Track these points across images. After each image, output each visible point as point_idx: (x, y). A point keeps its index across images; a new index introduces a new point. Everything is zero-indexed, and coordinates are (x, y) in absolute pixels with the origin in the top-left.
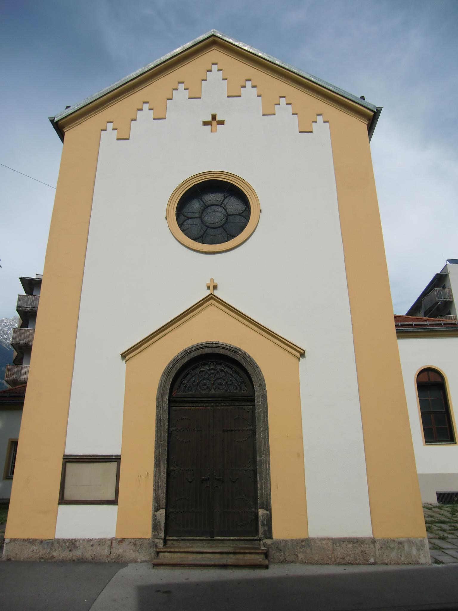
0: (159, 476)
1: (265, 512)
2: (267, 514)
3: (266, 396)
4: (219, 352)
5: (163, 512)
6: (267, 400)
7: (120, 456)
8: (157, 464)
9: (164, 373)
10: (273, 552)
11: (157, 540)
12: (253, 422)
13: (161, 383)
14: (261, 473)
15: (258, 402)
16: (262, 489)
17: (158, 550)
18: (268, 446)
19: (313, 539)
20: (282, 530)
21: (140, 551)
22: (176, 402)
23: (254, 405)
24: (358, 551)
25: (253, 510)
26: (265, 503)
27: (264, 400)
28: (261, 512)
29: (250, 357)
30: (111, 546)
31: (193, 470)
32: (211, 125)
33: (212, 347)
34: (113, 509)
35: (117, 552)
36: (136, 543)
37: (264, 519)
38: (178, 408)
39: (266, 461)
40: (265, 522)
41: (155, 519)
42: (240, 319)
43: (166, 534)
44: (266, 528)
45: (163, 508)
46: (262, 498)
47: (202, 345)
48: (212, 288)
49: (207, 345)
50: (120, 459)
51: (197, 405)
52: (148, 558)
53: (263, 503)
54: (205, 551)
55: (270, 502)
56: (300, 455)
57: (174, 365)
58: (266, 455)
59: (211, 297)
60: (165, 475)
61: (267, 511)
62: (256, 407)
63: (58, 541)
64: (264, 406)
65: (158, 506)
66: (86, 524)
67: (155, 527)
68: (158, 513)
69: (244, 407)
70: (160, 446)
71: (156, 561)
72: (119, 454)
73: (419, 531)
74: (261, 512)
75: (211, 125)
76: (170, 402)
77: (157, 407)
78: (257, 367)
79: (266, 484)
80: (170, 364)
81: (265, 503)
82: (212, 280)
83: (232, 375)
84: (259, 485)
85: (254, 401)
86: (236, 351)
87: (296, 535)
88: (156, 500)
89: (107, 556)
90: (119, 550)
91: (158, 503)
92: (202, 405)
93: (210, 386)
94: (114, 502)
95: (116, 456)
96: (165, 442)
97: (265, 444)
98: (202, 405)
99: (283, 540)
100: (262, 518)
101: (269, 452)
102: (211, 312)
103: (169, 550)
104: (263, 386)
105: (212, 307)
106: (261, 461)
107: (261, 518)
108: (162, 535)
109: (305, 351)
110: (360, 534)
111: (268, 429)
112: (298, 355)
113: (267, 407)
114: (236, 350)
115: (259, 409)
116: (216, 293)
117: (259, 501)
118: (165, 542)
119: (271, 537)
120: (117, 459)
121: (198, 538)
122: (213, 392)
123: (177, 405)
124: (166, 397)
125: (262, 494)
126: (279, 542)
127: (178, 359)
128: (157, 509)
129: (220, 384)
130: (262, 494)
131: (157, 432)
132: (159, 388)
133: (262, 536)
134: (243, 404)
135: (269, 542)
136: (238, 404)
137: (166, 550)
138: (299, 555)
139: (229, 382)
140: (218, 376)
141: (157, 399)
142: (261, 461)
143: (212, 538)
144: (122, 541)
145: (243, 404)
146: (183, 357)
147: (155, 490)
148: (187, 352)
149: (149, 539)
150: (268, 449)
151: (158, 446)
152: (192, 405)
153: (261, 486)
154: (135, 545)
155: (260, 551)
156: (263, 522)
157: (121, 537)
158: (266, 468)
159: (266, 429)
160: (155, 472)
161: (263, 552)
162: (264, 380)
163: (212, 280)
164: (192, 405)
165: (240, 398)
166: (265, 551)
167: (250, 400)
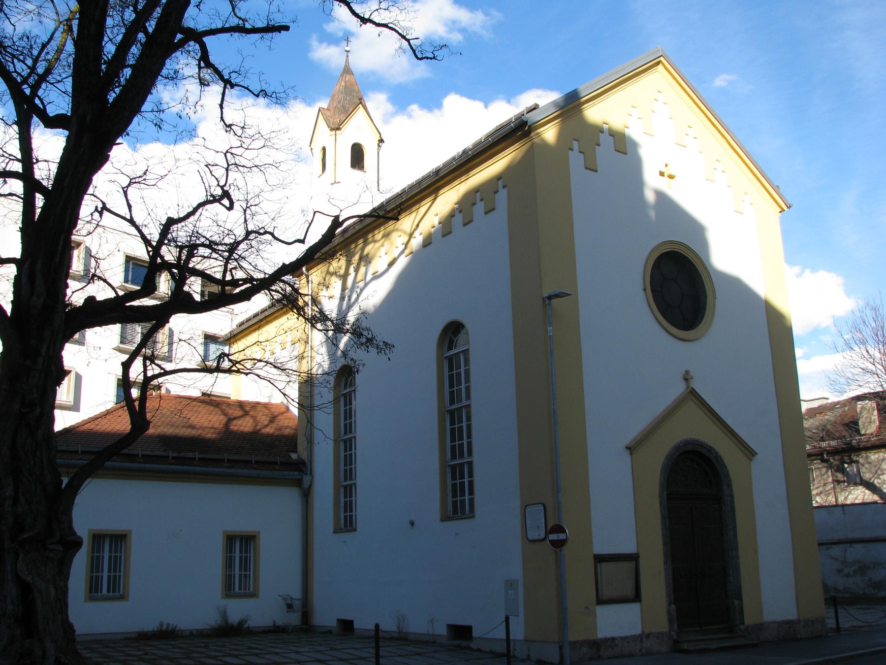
8: (666, 562)
20: (749, 619)
34: (635, 608)
63: (601, 640)
66: (618, 622)
67: (670, 621)
74: (736, 602)
135: (742, 627)
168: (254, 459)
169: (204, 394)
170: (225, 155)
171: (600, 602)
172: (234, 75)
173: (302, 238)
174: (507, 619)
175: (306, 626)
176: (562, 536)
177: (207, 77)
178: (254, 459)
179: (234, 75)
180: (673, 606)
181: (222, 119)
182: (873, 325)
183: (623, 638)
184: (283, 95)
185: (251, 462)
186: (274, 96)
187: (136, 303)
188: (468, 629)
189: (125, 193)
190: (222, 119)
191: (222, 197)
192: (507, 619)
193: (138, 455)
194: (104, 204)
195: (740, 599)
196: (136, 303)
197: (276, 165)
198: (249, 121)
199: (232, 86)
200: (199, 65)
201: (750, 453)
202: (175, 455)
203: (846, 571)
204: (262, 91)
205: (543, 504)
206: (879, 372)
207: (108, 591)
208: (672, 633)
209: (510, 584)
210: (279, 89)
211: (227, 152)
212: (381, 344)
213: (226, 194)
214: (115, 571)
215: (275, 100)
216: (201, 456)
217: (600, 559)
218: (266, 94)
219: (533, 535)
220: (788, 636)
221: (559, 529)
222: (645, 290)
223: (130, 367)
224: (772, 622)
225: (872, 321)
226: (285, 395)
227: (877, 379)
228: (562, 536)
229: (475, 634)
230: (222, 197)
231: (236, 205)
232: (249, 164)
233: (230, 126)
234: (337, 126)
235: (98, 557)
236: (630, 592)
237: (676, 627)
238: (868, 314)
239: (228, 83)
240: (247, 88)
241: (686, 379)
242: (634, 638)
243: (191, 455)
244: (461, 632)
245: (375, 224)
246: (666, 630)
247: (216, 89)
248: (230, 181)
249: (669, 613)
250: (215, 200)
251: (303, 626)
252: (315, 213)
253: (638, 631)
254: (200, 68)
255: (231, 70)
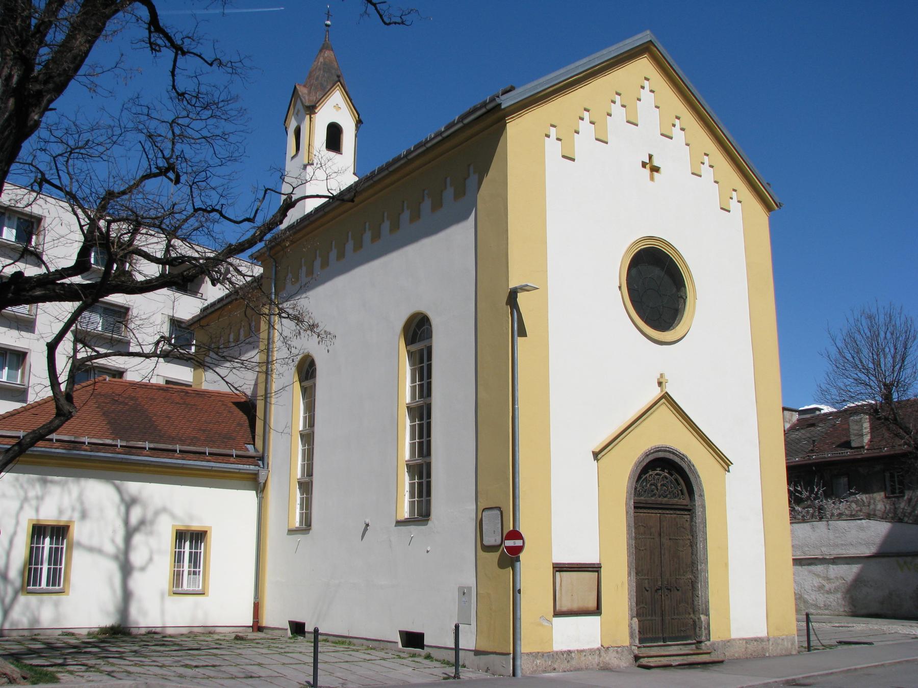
8: (629, 574)
12: (693, 533)
19: (734, 640)
20: (716, 635)
24: (760, 647)
32: (259, 487)
34: (596, 619)
36: (618, 649)
42: (606, 451)
63: (557, 653)
66: (577, 635)
67: (632, 635)
73: (795, 632)
74: (703, 617)
75: (259, 487)
87: (724, 637)
110: (760, 635)
135: (708, 643)
167: (689, 510)
168: (207, 450)
169: (168, 382)
170: (171, 125)
171: (557, 614)
172: (187, 41)
173: (252, 217)
174: (457, 627)
175: (257, 627)
176: (518, 543)
177: (160, 42)
178: (207, 450)
179: (187, 41)
180: (635, 620)
181: (174, 87)
182: (868, 334)
183: (580, 652)
184: (239, 65)
185: (205, 453)
186: (229, 65)
187: (67, 281)
188: (421, 636)
189: (265, 193)
190: (174, 87)
191: (167, 170)
192: (457, 627)
193: (84, 443)
194: (43, 174)
195: (707, 615)
196: (67, 281)
197: (224, 136)
198: (203, 89)
199: (184, 53)
200: (149, 29)
201: (726, 463)
202: (124, 444)
203: (827, 587)
204: (215, 60)
205: (499, 508)
206: (872, 384)
207: (48, 585)
208: (633, 647)
209: (464, 592)
210: (235, 58)
211: (173, 121)
212: (322, 332)
213: (171, 168)
214: (56, 564)
215: (230, 70)
216: (152, 446)
217: (560, 568)
218: (221, 63)
219: (490, 540)
220: (755, 654)
221: (515, 534)
222: (620, 287)
223: (56, 348)
224: (740, 639)
225: (867, 331)
226: (227, 383)
227: (870, 391)
228: (518, 543)
229: (427, 641)
230: (167, 170)
231: (183, 179)
232: (197, 135)
233: (183, 94)
234: (312, 104)
235: (38, 548)
236: (592, 604)
237: (637, 641)
238: (864, 324)
239: (179, 50)
240: (200, 56)
241: (660, 384)
242: (592, 652)
243: (140, 444)
244: (413, 640)
245: (331, 207)
246: (627, 643)
247: (168, 54)
248: (177, 153)
249: (630, 626)
250: (163, 172)
251: (118, 635)
252: (266, 191)
253: (597, 645)
254: (150, 32)
255: (185, 34)
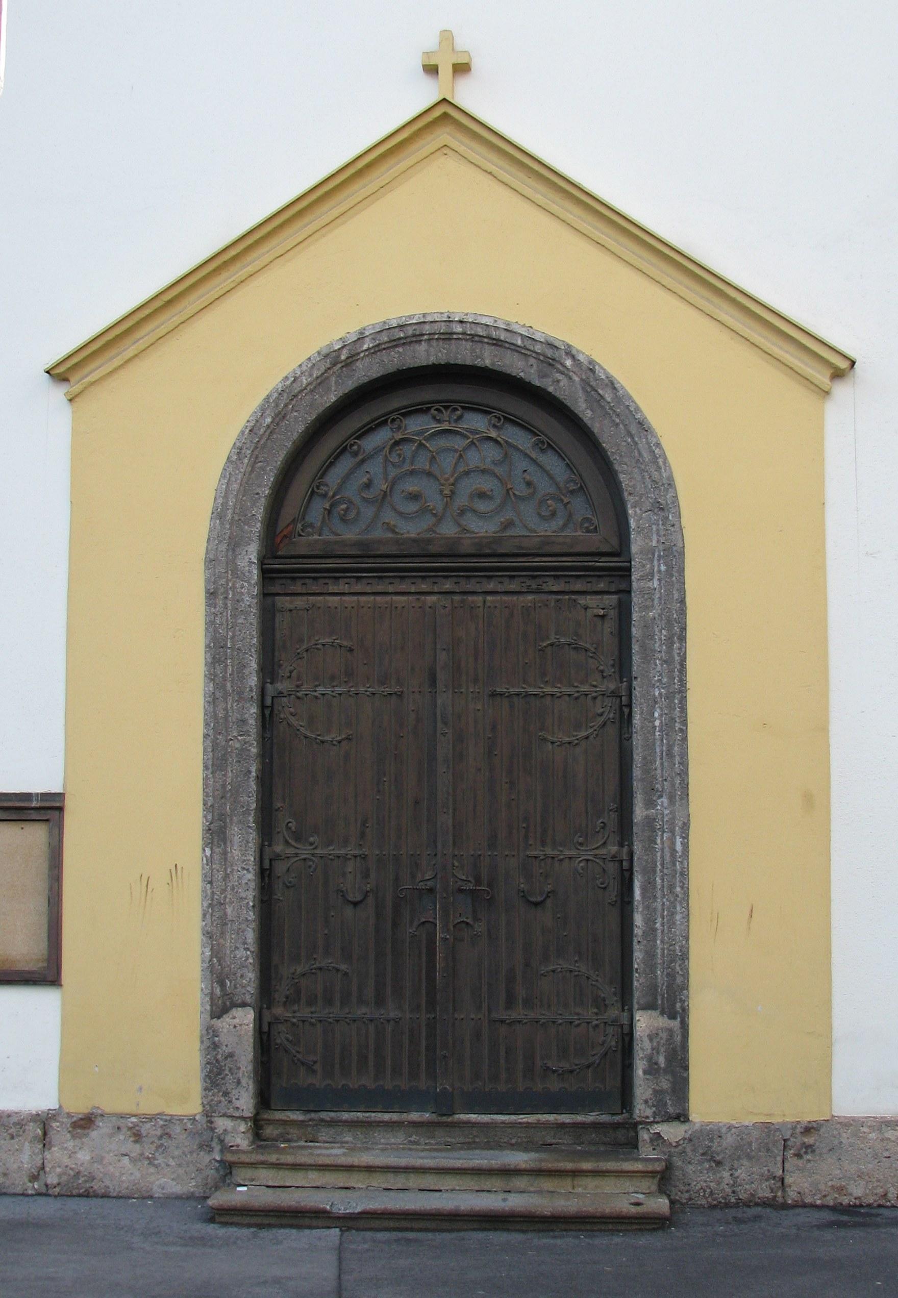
0: (226, 877)
1: (663, 1022)
2: (670, 1031)
3: (682, 554)
4: (478, 362)
5: (245, 1018)
6: (682, 571)
7: (60, 796)
8: (216, 834)
9: (239, 450)
10: (690, 1169)
11: (222, 1124)
13: (224, 495)
14: (650, 871)
15: (645, 580)
16: (651, 931)
17: (229, 1157)
18: (684, 763)
20: (728, 1079)
21: (160, 1160)
22: (293, 575)
23: (629, 592)
25: (614, 1012)
26: (662, 988)
27: (670, 567)
28: (645, 1023)
29: (612, 384)
30: (45, 1140)
31: (364, 857)
33: (448, 337)
34: (37, 1006)
35: (66, 1161)
37: (656, 1050)
38: (299, 602)
39: (672, 822)
40: (662, 1060)
41: (215, 1046)
43: (264, 1100)
44: (665, 1084)
45: (244, 1005)
46: (651, 967)
47: (401, 327)
48: (446, 71)
49: (427, 329)
50: (61, 809)
51: (380, 588)
52: (191, 1186)
53: (653, 988)
54: (418, 1162)
55: (685, 987)
56: (814, 802)
57: (280, 417)
58: (672, 799)
59: (444, 116)
60: (250, 876)
61: (672, 1017)
62: (636, 599)
64: (669, 593)
65: (225, 994)
67: (216, 1073)
68: (224, 1024)
69: (582, 600)
70: (224, 758)
71: (219, 1199)
72: (57, 789)
76: (267, 574)
77: (211, 595)
78: (643, 426)
79: (672, 914)
80: (263, 409)
81: (662, 988)
82: (447, 37)
83: (534, 461)
84: (638, 919)
85: (626, 573)
86: (551, 355)
88: (218, 973)
89: (34, 1178)
90: (69, 1156)
91: (222, 984)
92: (403, 587)
93: (435, 502)
94: (47, 975)
95: (46, 796)
96: (249, 741)
97: (670, 755)
98: (403, 587)
99: (730, 1127)
100: (647, 1045)
101: (685, 786)
102: (447, 182)
103: (273, 1158)
104: (665, 508)
105: (450, 164)
106: (650, 822)
107: (642, 1048)
108: (245, 1101)
109: (853, 363)
111: (683, 690)
112: (822, 377)
113: (683, 601)
114: (549, 352)
115: (647, 608)
116: (470, 97)
117: (638, 982)
118: (257, 1125)
119: (682, 1117)
120: (43, 810)
121: (386, 1117)
122: (448, 530)
123: (298, 587)
124: (251, 553)
125: (650, 955)
126: (712, 1133)
127: (297, 388)
128: (220, 1007)
129: (482, 495)
130: (650, 955)
131: (212, 700)
132: (219, 515)
133: (649, 1112)
134: (578, 586)
135: (672, 1132)
136: (448, 586)
137: (261, 1158)
138: (789, 1180)
139: (521, 490)
140: (473, 459)
141: (211, 562)
142: (650, 822)
143: (444, 1119)
144: (85, 1123)
145: (578, 586)
146: (321, 382)
147: (208, 935)
148: (338, 360)
149: (193, 1120)
150: (684, 774)
151: (217, 760)
152: (358, 588)
153: (650, 922)
154: (138, 1137)
155: (639, 1166)
156: (651, 1060)
157: (79, 1106)
158: (673, 851)
159: (678, 694)
160: (210, 861)
161: (650, 1168)
162: (671, 484)
163: (447, 37)
164: (358, 588)
165: (567, 561)
166: (658, 1167)
167: (610, 568)
